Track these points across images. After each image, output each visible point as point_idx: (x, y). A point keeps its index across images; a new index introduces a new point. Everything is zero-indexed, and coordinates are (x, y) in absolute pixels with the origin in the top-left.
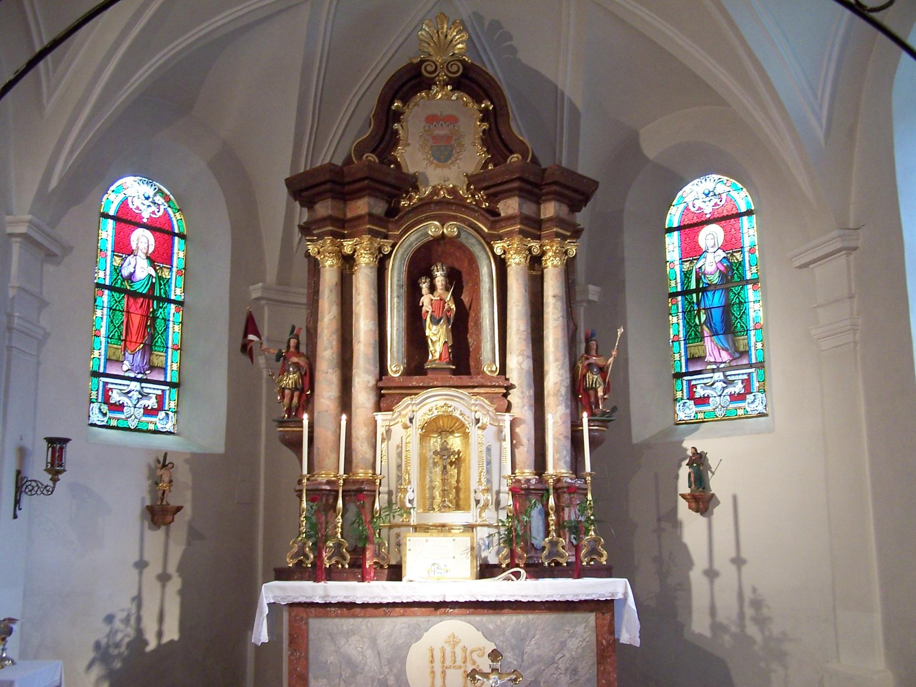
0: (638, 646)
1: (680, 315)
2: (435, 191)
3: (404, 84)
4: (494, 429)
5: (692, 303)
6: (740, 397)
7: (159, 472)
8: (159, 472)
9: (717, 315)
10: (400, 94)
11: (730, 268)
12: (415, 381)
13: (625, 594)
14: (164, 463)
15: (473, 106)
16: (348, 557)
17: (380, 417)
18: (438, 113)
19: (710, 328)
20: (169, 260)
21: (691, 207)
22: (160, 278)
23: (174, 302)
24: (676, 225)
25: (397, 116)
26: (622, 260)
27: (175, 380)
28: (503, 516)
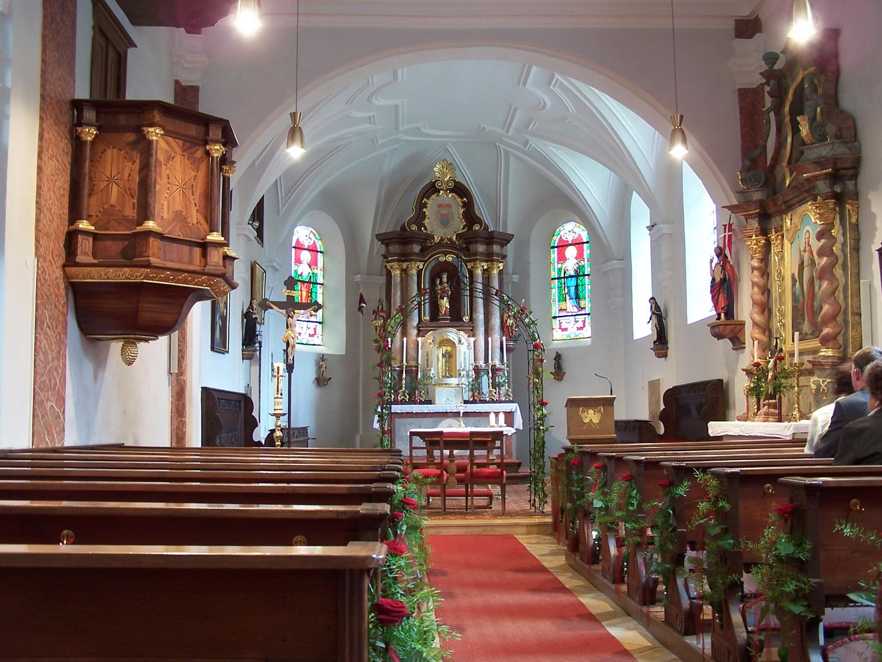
0: (522, 429)
1: (557, 289)
2: (442, 240)
3: (427, 191)
4: (467, 344)
5: (561, 283)
6: (581, 328)
7: (321, 363)
8: (321, 363)
9: (572, 290)
10: (426, 196)
11: (579, 268)
12: (434, 324)
13: (516, 409)
14: (322, 358)
15: (459, 200)
16: (408, 397)
17: (420, 339)
18: (443, 203)
19: (569, 296)
20: (316, 264)
21: (562, 237)
22: (313, 273)
23: (320, 284)
24: (556, 245)
25: (425, 205)
26: (529, 263)
27: (321, 321)
28: (470, 380)
